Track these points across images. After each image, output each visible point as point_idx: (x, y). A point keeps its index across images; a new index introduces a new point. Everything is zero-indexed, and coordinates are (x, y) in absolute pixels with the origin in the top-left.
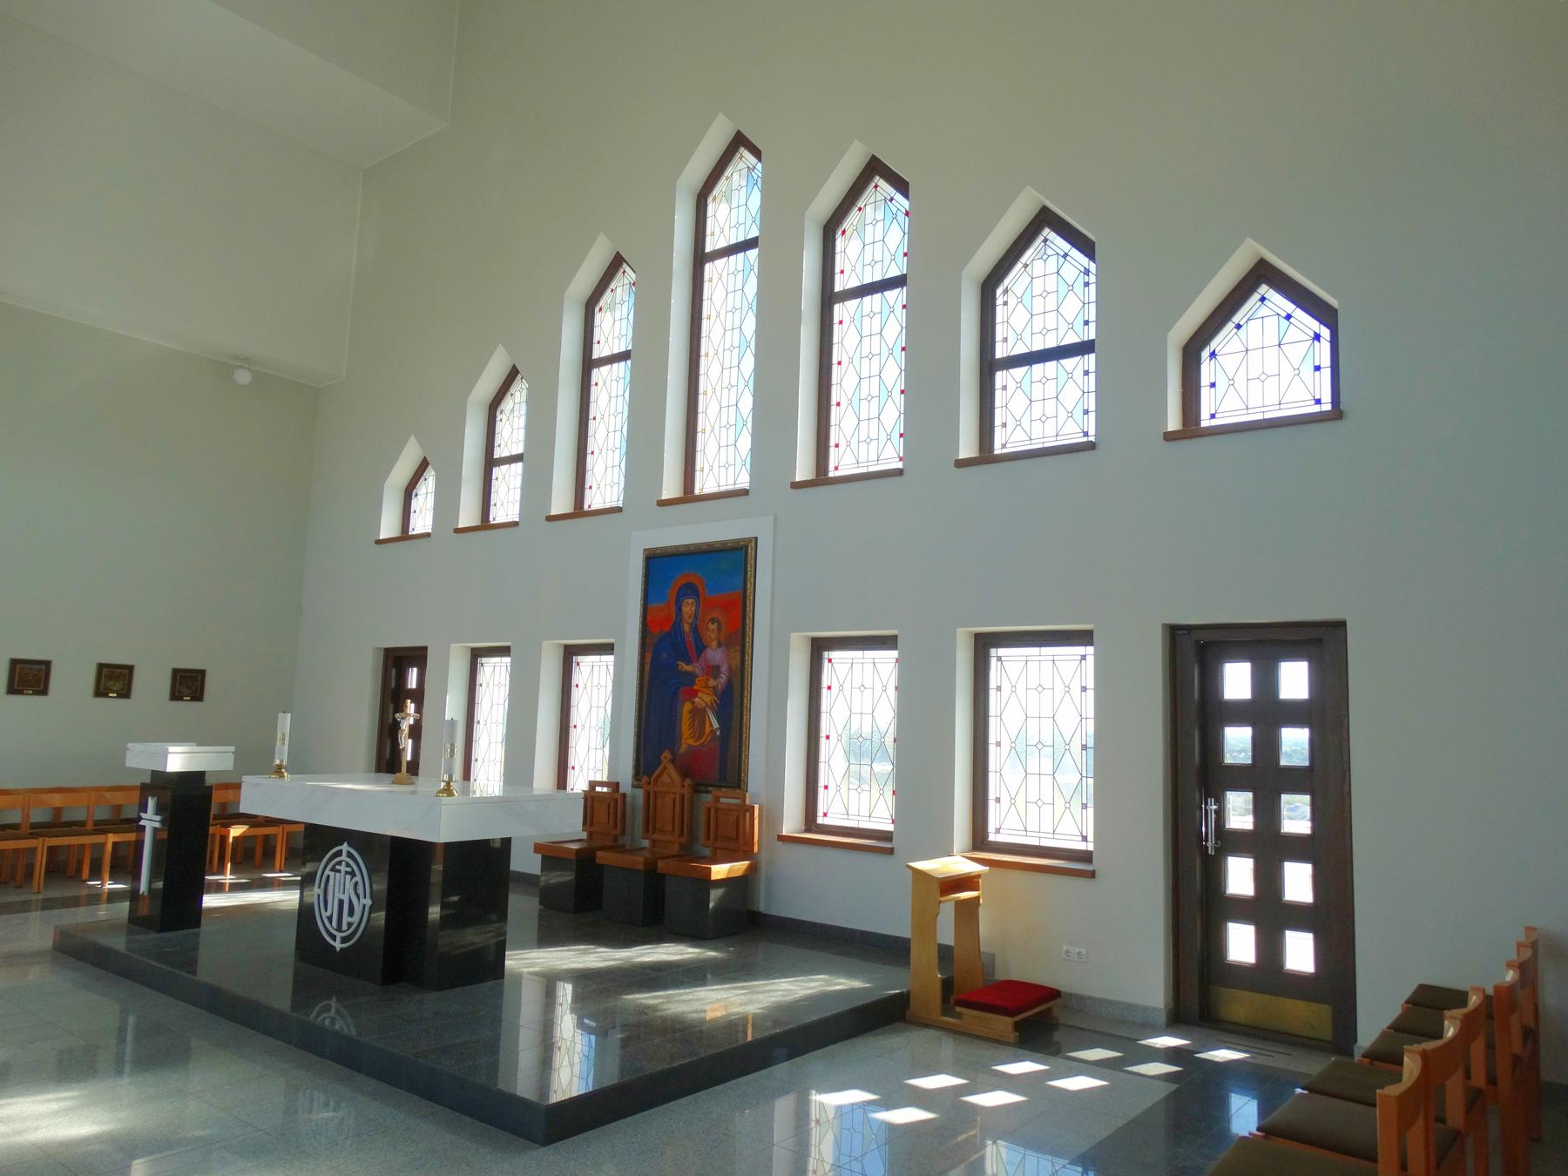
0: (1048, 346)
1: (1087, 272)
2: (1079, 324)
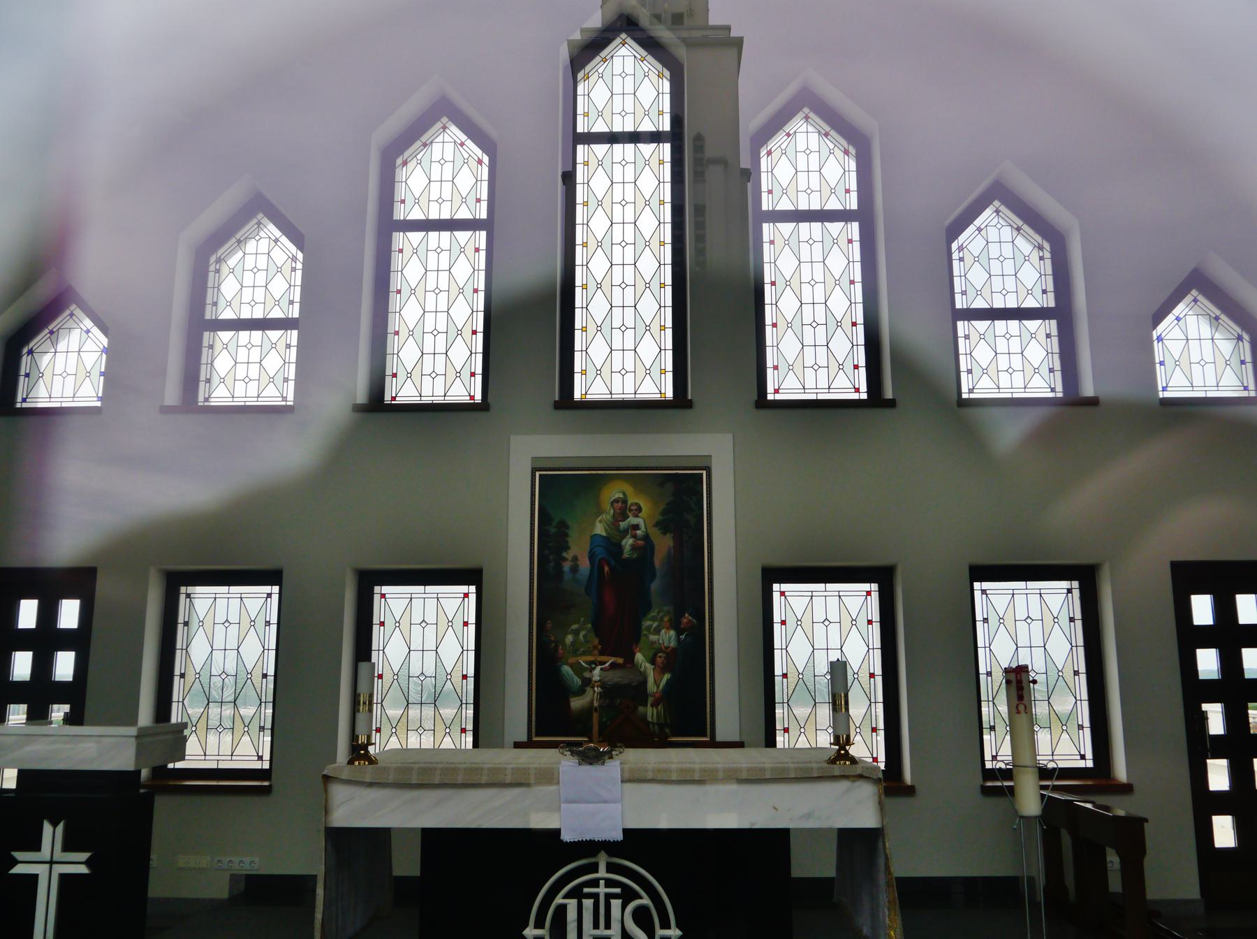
0: (1009, 306)
1: (294, 259)
2: (284, 303)
